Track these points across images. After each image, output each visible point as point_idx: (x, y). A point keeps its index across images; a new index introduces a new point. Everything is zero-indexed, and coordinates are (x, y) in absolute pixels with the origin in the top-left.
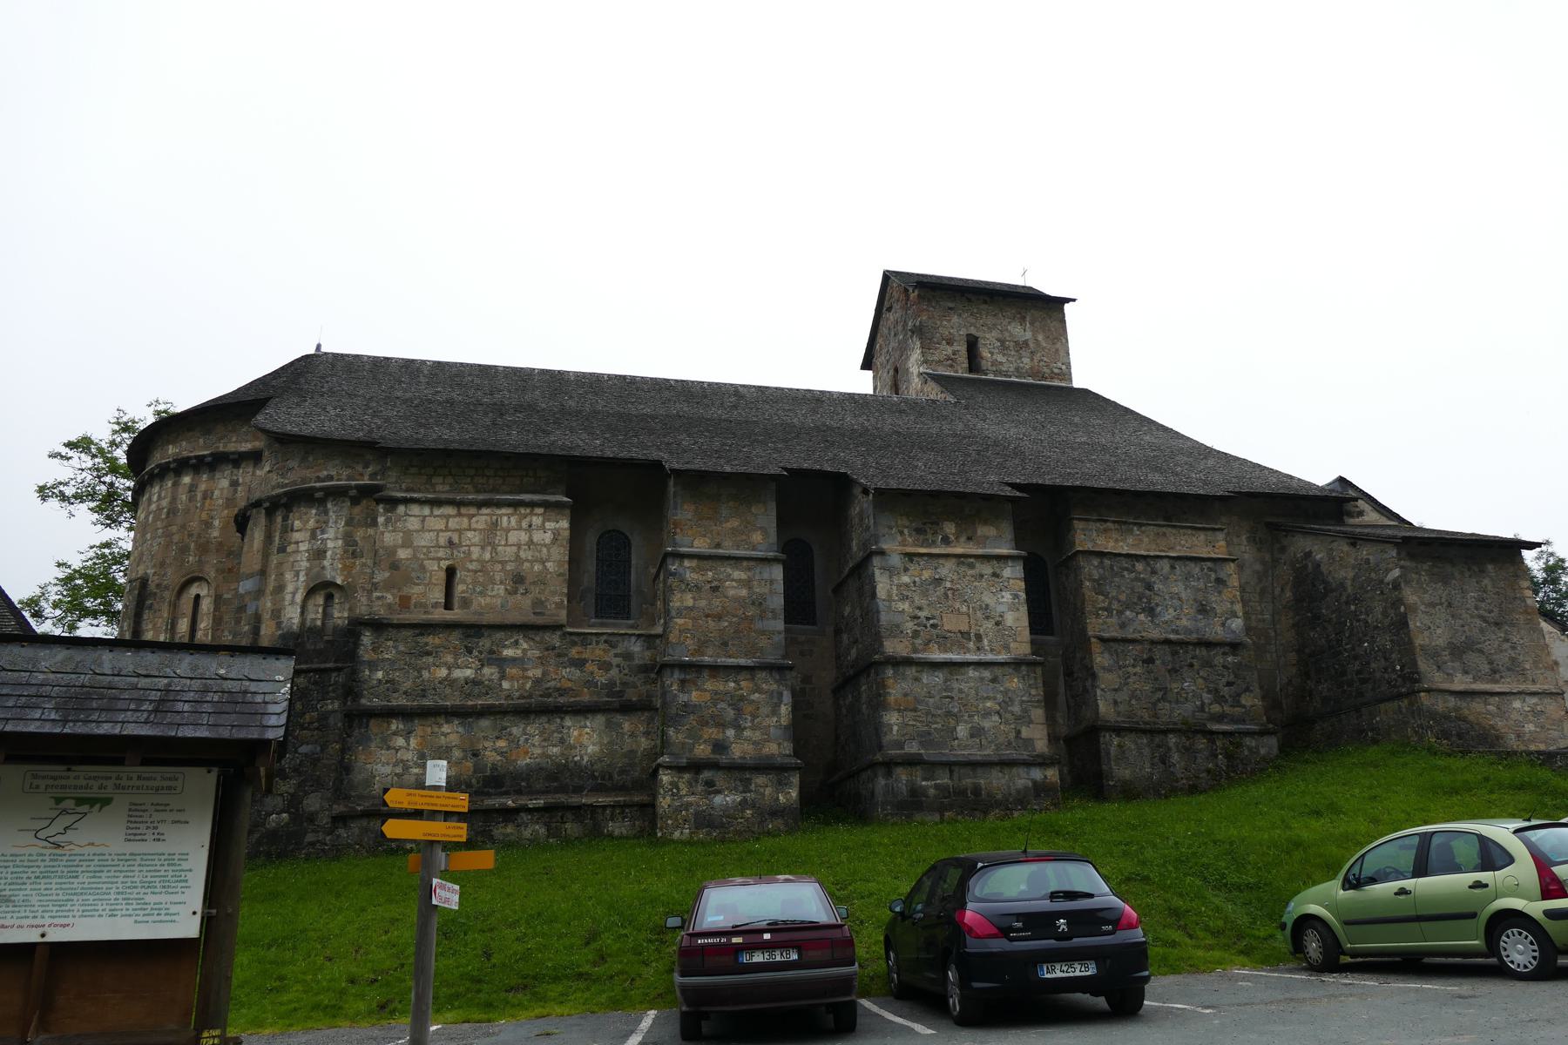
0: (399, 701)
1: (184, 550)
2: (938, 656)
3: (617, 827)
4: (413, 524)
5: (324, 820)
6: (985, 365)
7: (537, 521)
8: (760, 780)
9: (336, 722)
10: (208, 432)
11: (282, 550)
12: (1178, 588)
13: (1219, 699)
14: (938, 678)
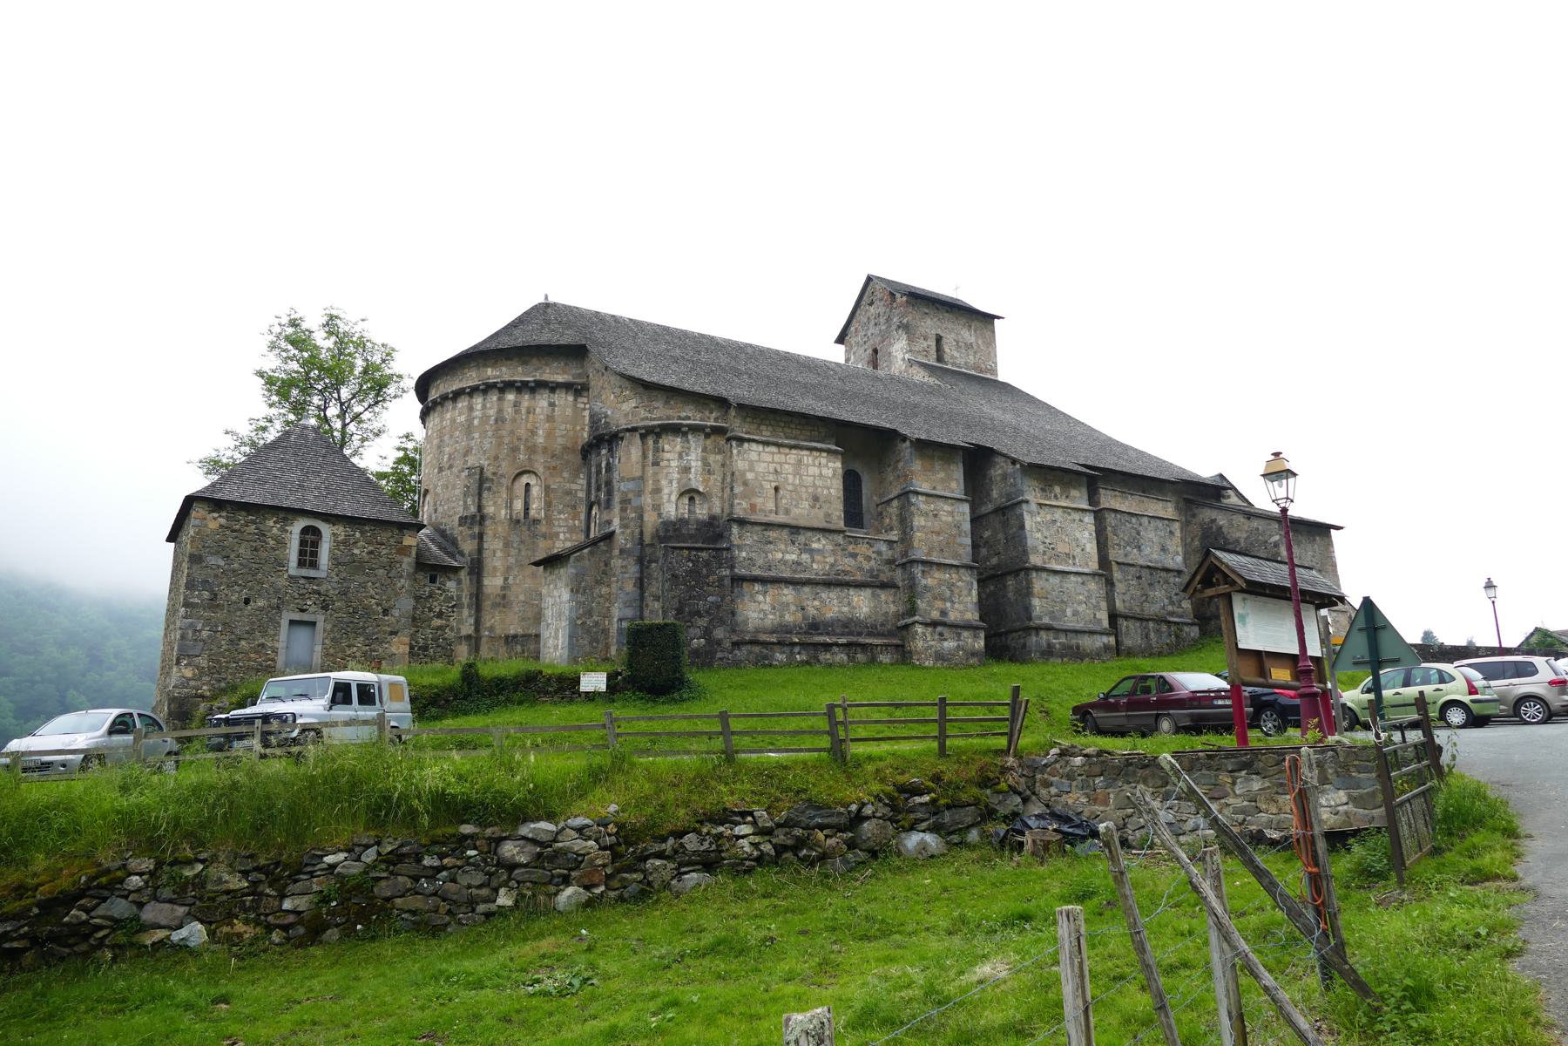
0: (756, 572)
1: (515, 450)
2: (1059, 568)
3: (885, 658)
4: (754, 456)
5: (727, 644)
6: (947, 357)
7: (823, 461)
8: (965, 634)
9: (727, 582)
10: (525, 363)
11: (656, 464)
12: (1152, 535)
13: (1172, 603)
14: (1055, 580)
